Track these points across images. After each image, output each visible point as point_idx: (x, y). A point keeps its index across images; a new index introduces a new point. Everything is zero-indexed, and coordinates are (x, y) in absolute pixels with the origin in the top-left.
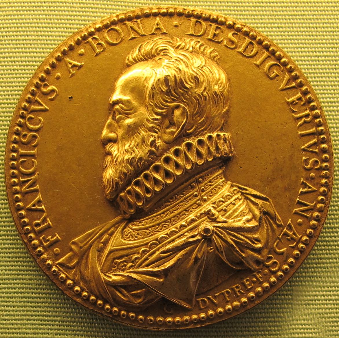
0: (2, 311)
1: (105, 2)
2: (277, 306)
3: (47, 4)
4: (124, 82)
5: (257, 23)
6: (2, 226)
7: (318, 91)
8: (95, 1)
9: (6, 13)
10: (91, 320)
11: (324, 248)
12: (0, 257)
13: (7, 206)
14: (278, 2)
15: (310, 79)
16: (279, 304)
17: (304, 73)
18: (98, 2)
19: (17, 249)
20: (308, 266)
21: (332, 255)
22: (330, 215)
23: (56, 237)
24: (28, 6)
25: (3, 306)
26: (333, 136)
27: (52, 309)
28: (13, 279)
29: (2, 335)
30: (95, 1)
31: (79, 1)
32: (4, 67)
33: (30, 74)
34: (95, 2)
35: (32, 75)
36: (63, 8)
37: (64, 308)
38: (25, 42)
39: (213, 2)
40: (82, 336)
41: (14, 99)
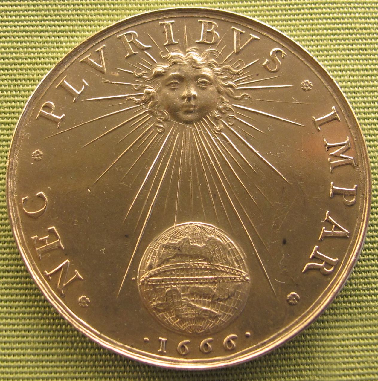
0: (3, 373)
1: (17, 2)
2: (293, 374)
3: (352, 5)
6: (2, 307)
9: (10, 23)
10: (99, 356)
12: (0, 265)
13: (7, 221)
14: (164, 3)
18: (22, 2)
19: (24, 325)
24: (52, 10)
25: (4, 367)
27: (56, 345)
30: (267, 2)
31: (113, 2)
34: (17, 2)
36: (341, 37)
38: (16, 34)
40: (91, 378)
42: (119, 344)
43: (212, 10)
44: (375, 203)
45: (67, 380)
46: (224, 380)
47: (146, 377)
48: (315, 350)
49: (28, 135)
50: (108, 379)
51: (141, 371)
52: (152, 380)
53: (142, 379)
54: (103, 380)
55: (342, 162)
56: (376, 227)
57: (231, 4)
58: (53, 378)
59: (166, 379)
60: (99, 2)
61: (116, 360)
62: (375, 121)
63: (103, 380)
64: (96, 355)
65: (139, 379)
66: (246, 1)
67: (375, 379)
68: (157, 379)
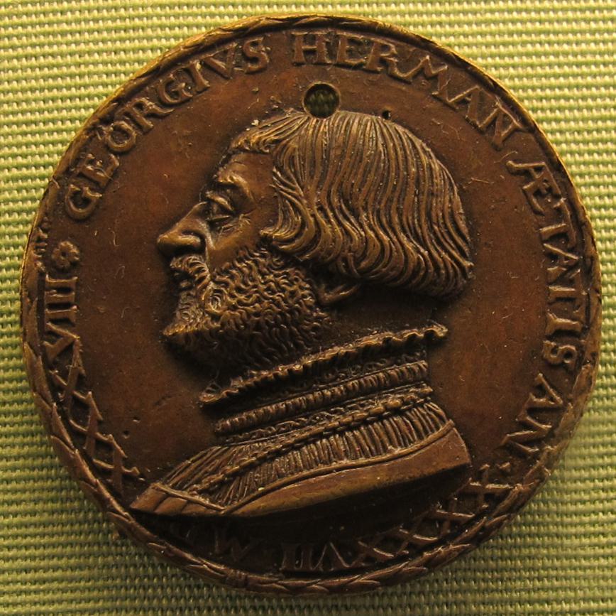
4: (443, 469)
5: (506, 67)
7: (595, 212)
8: (74, 3)
11: (591, 485)
15: (588, 201)
16: (492, 559)
17: (546, 131)
20: (554, 507)
21: (588, 482)
22: (604, 364)
23: (134, 109)
26: (601, 240)
28: (19, 571)
29: (610, 3)
30: (74, 3)
32: (20, 115)
33: (42, 178)
35: (47, 181)
37: (126, 589)
39: (215, 5)
41: (72, 120)
42: (356, 577)
43: (458, 260)
44: (609, 513)
45: (110, 615)
46: (460, 613)
47: (214, 608)
48: (499, 554)
49: (183, 301)
50: (123, 612)
51: (166, 597)
52: (306, 612)
53: (187, 612)
54: (150, 614)
55: (568, 324)
56: (612, 333)
57: (384, 7)
58: (602, 612)
59: (251, 612)
60: (97, 5)
61: (145, 577)
62: (610, 146)
63: (150, 614)
64: (135, 566)
65: (311, 611)
66: (422, 3)
67: (570, 612)
68: (214, 611)
